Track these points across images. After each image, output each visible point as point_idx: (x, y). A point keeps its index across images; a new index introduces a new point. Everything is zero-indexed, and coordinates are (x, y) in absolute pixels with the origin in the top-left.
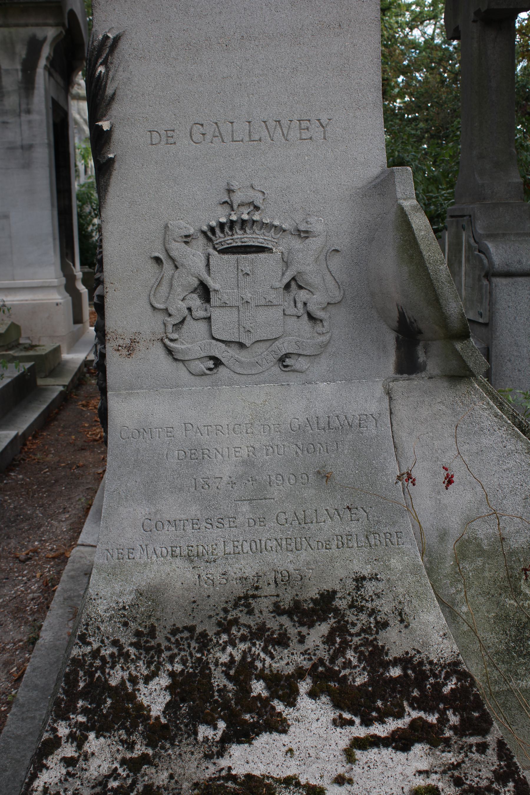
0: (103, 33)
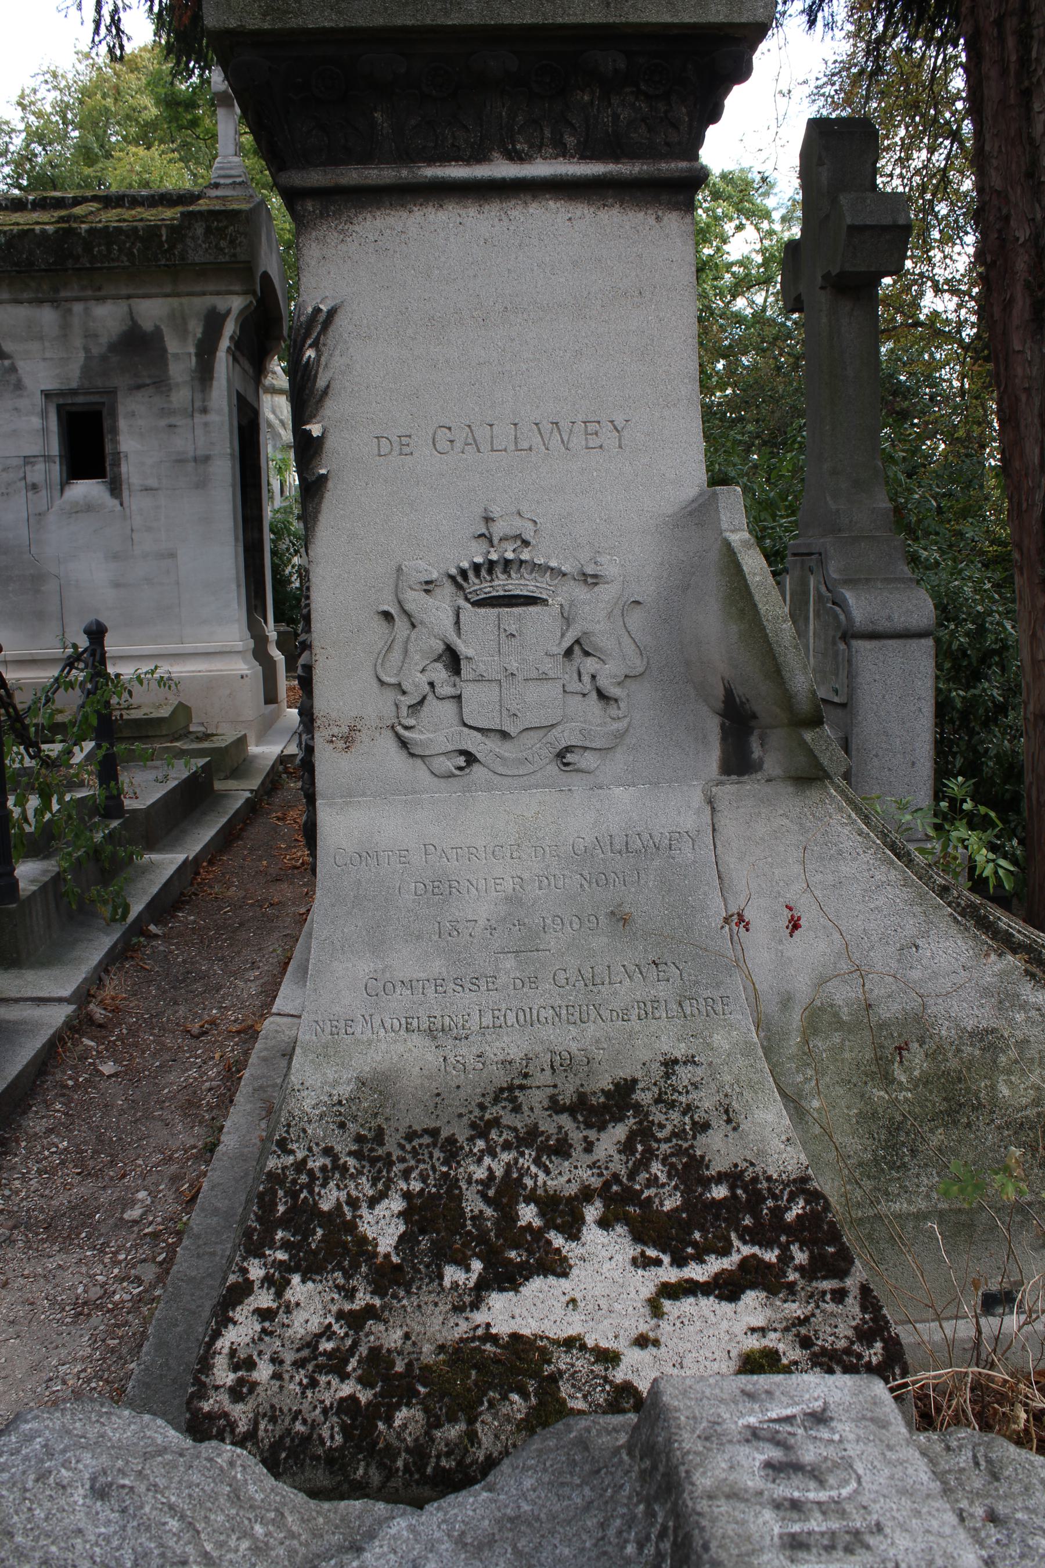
0: (314, 304)
